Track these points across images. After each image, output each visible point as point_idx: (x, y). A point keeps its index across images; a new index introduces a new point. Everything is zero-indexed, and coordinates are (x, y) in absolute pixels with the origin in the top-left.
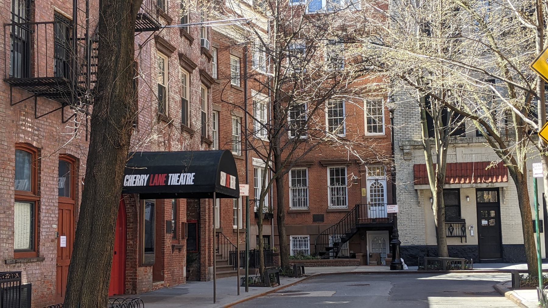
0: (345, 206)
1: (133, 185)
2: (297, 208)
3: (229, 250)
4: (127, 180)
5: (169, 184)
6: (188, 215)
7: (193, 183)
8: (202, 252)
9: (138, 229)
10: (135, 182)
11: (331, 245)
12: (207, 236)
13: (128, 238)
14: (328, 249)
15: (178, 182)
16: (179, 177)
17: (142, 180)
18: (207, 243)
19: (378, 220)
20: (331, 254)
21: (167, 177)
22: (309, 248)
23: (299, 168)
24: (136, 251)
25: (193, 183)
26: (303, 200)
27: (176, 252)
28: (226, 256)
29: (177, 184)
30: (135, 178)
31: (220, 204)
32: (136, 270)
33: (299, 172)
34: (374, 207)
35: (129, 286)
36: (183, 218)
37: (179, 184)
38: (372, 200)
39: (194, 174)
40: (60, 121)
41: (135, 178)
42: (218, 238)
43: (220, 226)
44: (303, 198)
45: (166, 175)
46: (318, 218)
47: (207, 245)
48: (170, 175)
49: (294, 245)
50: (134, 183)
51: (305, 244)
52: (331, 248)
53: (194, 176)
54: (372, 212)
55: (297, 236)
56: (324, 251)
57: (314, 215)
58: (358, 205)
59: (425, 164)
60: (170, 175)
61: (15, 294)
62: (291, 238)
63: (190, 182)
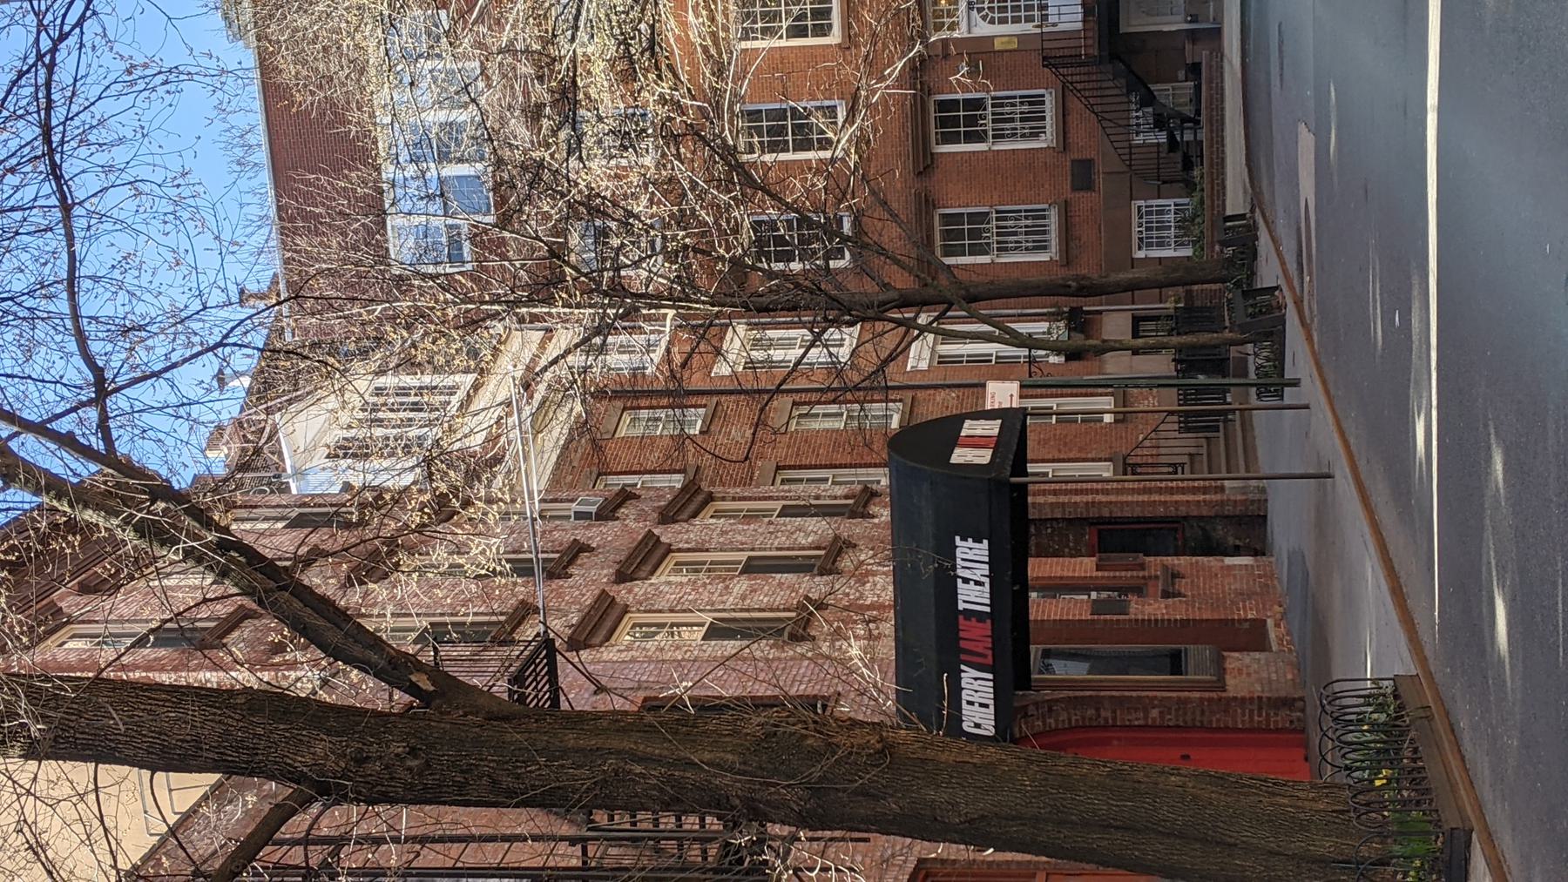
0: (1047, 99)
4: (977, 726)
5: (988, 609)
7: (986, 542)
8: (1183, 511)
11: (1162, 138)
12: (1134, 499)
14: (1173, 144)
16: (966, 581)
20: (1188, 136)
22: (1171, 202)
23: (937, 236)
25: (986, 542)
27: (1182, 585)
28: (1192, 442)
33: (947, 235)
34: (1050, 10)
35: (1281, 718)
36: (1084, 566)
37: (987, 580)
38: (1029, 19)
39: (957, 538)
41: (971, 703)
42: (1140, 465)
44: (1024, 222)
46: (1083, 175)
48: (961, 606)
49: (1161, 245)
50: (986, 706)
52: (1171, 137)
53: (964, 539)
54: (1063, 18)
55: (1135, 237)
56: (1178, 157)
57: (1075, 189)
58: (1044, 58)
60: (961, 606)
62: (1141, 254)
63: (981, 550)
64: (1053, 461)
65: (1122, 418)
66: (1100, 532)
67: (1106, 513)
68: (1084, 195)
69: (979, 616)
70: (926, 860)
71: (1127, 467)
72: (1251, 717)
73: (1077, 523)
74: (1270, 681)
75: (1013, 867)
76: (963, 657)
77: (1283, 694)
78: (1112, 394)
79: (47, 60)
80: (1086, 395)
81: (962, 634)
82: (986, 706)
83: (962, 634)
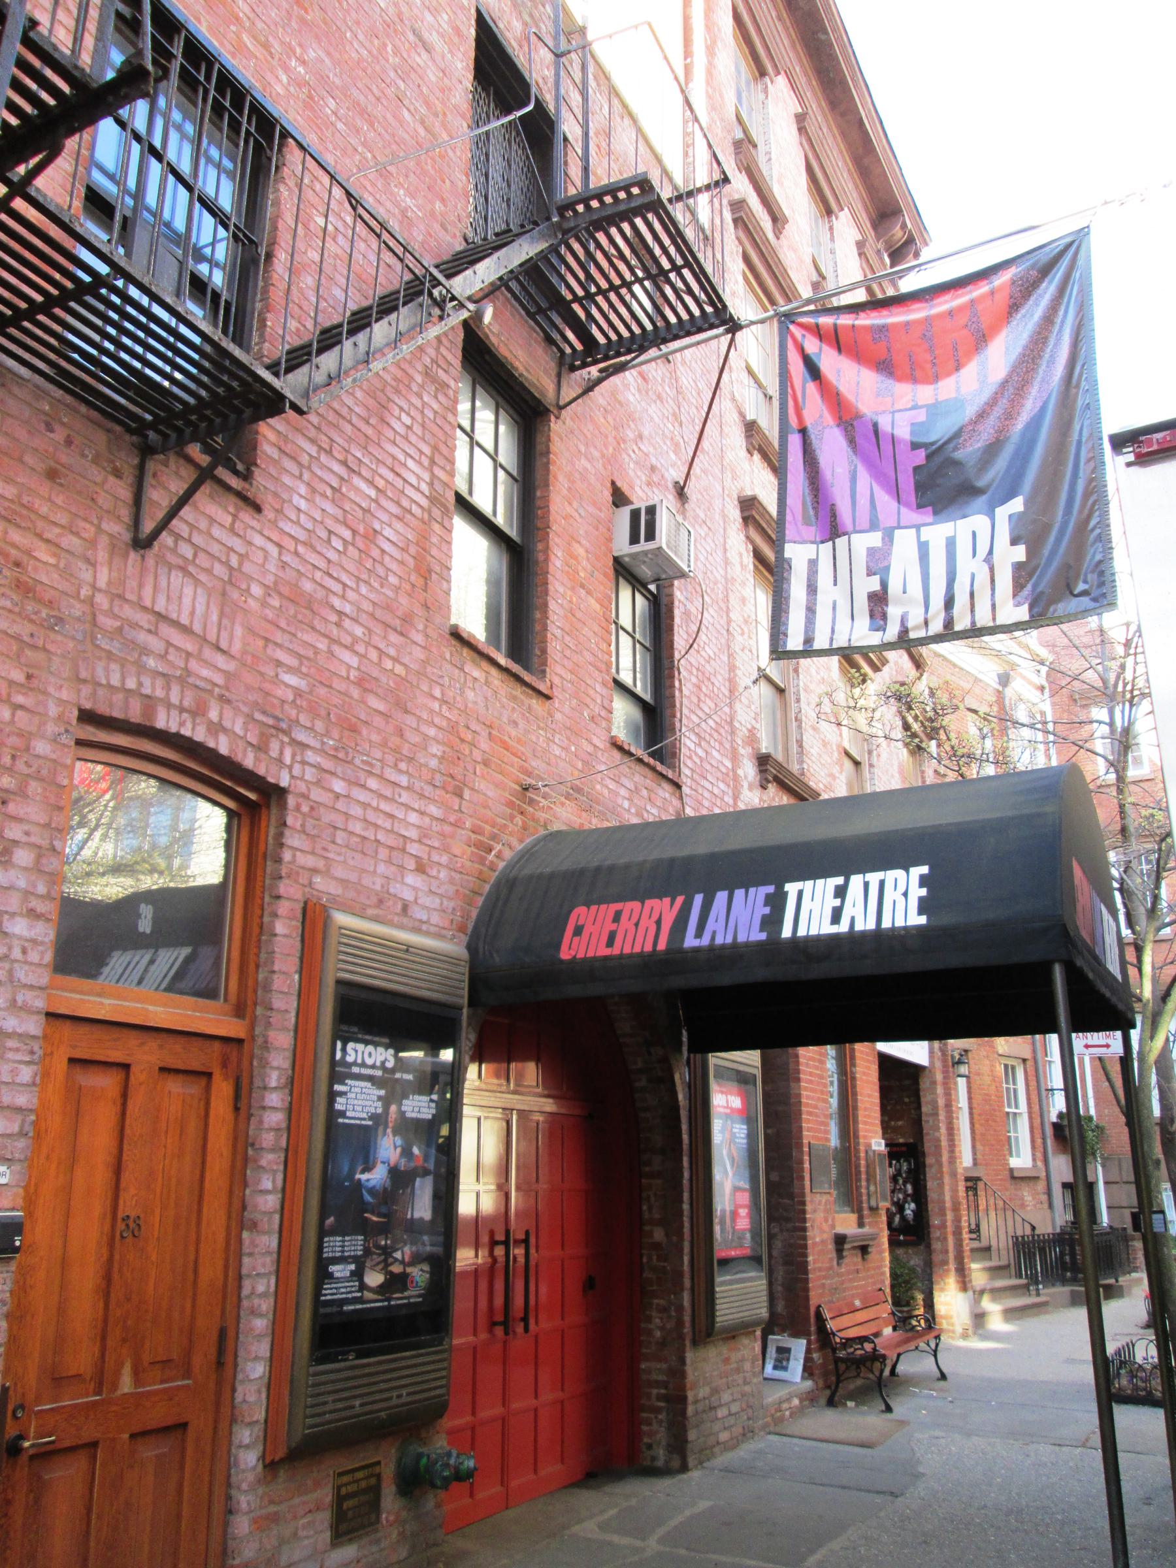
1: (603, 951)
3: (1011, 1233)
4: (578, 931)
5: (786, 933)
6: (886, 1128)
7: (922, 920)
8: (937, 1246)
9: (686, 1182)
12: (946, 1191)
13: (646, 1216)
16: (841, 892)
17: (648, 924)
18: (949, 1216)
21: (777, 902)
24: (681, 1274)
25: (922, 920)
27: (852, 1259)
28: (1002, 1245)
29: (834, 929)
31: (970, 1099)
32: (682, 1361)
39: (925, 869)
40: (118, 529)
41: (617, 917)
42: (976, 1195)
43: (975, 1159)
45: (771, 889)
47: (949, 1223)
48: (792, 888)
50: (610, 942)
53: (924, 881)
60: (792, 888)
64: (971, 1108)
65: (1016, 1178)
66: (49, 995)
67: (930, 1160)
69: (773, 921)
70: (283, 806)
71: (973, 1183)
72: (658, 1384)
74: (713, 1408)
76: (698, 899)
77: (692, 1435)
78: (1035, 1166)
80: (1033, 1141)
82: (610, 942)
83: (739, 893)
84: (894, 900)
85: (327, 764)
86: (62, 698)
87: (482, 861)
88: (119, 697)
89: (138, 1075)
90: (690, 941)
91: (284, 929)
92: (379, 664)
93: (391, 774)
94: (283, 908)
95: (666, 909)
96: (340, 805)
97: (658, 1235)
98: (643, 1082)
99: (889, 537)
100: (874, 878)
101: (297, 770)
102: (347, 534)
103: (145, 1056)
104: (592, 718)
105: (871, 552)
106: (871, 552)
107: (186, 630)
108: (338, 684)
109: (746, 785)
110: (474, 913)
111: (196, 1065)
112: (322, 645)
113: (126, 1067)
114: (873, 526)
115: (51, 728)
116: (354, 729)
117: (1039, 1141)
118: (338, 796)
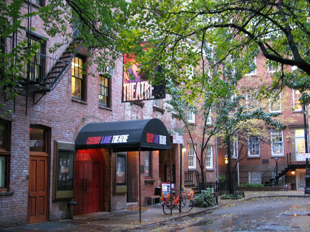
1: (92, 144)
2: (253, 156)
4: (89, 141)
5: (112, 143)
10: (118, 140)
15: (118, 141)
16: (119, 137)
17: (97, 140)
19: (302, 163)
21: (112, 138)
25: (126, 142)
26: (256, 151)
30: (119, 137)
34: (301, 154)
37: (118, 142)
39: (128, 135)
43: (197, 167)
44: (256, 149)
48: (114, 136)
50: (93, 143)
51: (258, 177)
52: (273, 180)
53: (128, 137)
54: (299, 157)
57: (263, 160)
58: (290, 154)
59: (109, 108)
60: (114, 136)
61: (193, 178)
63: (125, 141)
67: (176, 168)
68: (262, 162)
69: (111, 141)
73: (6, 164)
75: (293, 143)
76: (103, 137)
79: (79, 13)
81: (108, 137)
84: (123, 139)
85: (56, 123)
86: (28, 124)
87: (77, 130)
88: (35, 122)
89: (37, 161)
90: (102, 143)
91: (52, 144)
92: (62, 108)
93: (64, 122)
94: (52, 141)
95: (99, 138)
96: (58, 127)
97: (107, 179)
98: (105, 157)
99: (137, 83)
100: (123, 136)
101: (53, 125)
102: (57, 92)
103: (38, 159)
104: (95, 104)
105: (134, 86)
106: (134, 86)
107: (40, 112)
108: (57, 112)
109: (127, 106)
110: (76, 137)
111: (43, 159)
112: (55, 108)
113: (36, 160)
114: (135, 82)
115: (28, 127)
116: (59, 118)
117: (215, 163)
118: (57, 126)
